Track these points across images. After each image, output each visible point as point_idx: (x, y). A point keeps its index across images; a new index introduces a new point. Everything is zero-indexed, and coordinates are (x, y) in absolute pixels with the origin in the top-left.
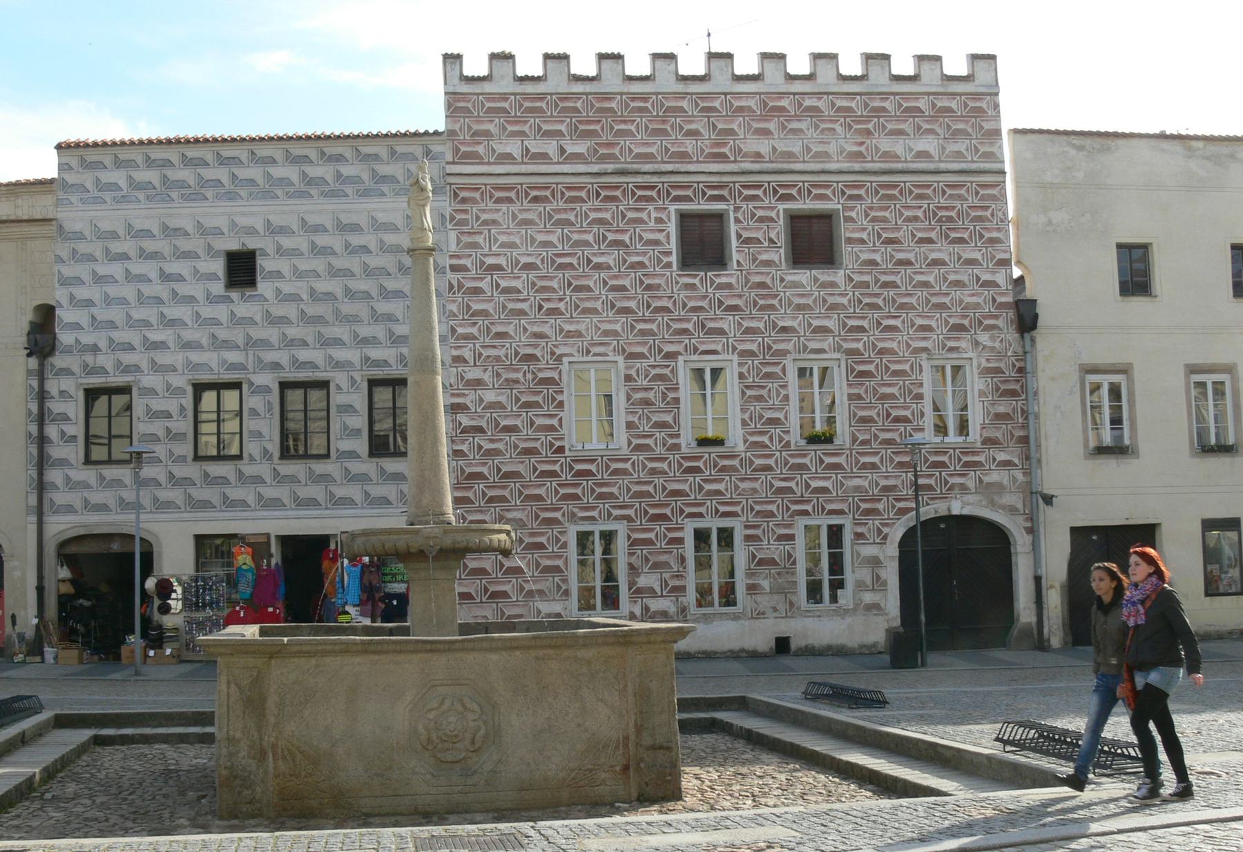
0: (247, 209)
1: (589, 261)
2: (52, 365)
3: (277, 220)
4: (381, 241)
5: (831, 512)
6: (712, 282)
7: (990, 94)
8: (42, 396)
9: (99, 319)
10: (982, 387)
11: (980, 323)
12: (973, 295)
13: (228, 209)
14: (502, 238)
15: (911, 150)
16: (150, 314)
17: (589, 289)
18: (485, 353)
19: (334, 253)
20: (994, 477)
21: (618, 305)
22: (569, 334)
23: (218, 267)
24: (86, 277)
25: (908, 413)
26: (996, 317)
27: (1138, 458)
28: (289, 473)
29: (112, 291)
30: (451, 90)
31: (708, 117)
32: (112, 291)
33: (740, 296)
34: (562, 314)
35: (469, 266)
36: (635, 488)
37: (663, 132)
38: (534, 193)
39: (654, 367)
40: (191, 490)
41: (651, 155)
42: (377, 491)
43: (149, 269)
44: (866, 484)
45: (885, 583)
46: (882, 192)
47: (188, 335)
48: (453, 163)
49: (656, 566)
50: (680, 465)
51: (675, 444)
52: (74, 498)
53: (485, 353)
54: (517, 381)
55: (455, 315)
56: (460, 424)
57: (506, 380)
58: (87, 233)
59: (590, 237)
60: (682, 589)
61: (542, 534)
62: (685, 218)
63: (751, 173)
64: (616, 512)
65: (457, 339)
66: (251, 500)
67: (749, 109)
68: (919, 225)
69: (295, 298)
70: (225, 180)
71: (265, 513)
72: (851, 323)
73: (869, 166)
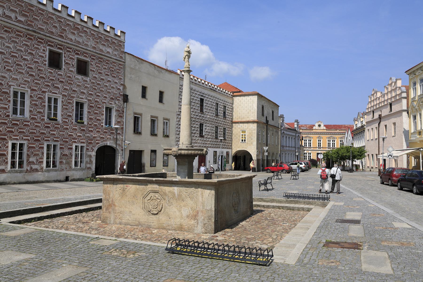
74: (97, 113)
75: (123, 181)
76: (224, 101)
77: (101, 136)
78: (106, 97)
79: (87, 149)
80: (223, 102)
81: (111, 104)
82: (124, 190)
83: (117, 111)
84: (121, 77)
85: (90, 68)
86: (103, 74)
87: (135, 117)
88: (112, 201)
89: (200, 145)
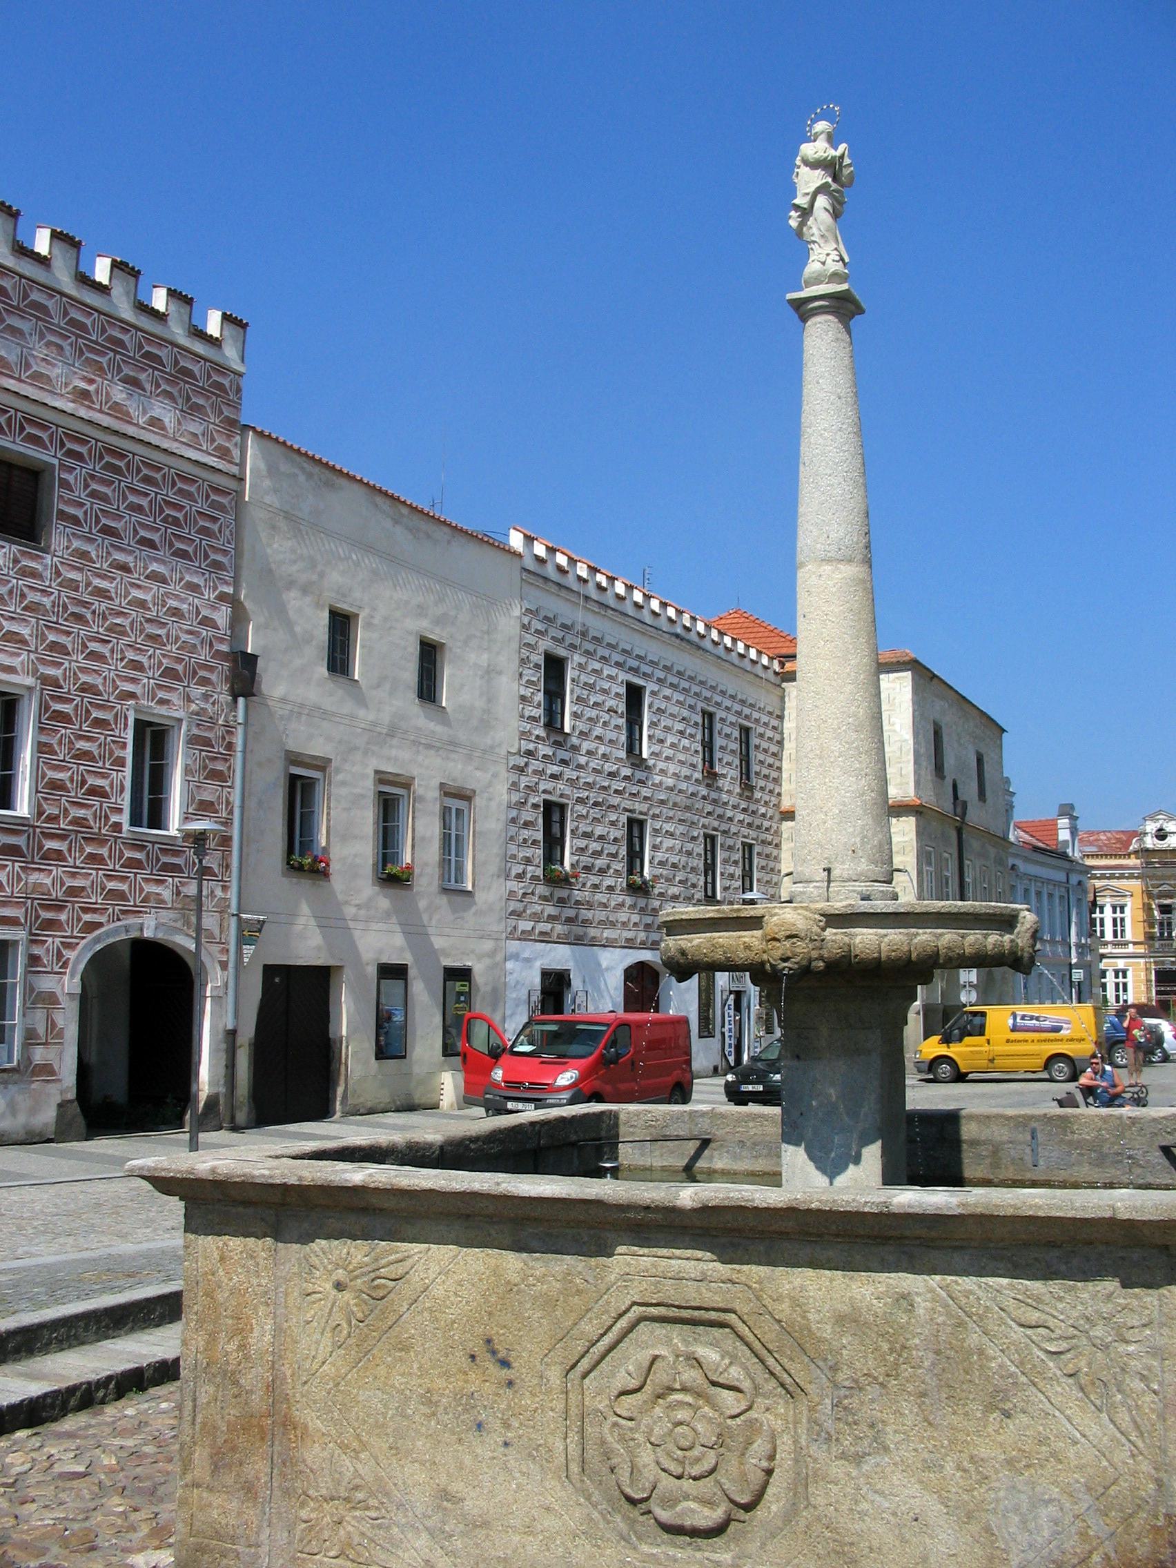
27: (284, 875)
44: (48, 881)
45: (60, 1034)
74: (85, 755)
75: (365, 1210)
76: (743, 702)
77: (111, 885)
78: (137, 666)
79: (34, 960)
80: (737, 707)
81: (162, 702)
82: (376, 1296)
83: (193, 740)
84: (219, 558)
85: (58, 505)
86: (128, 540)
87: (293, 779)
88: (271, 1388)
89: (630, 935)
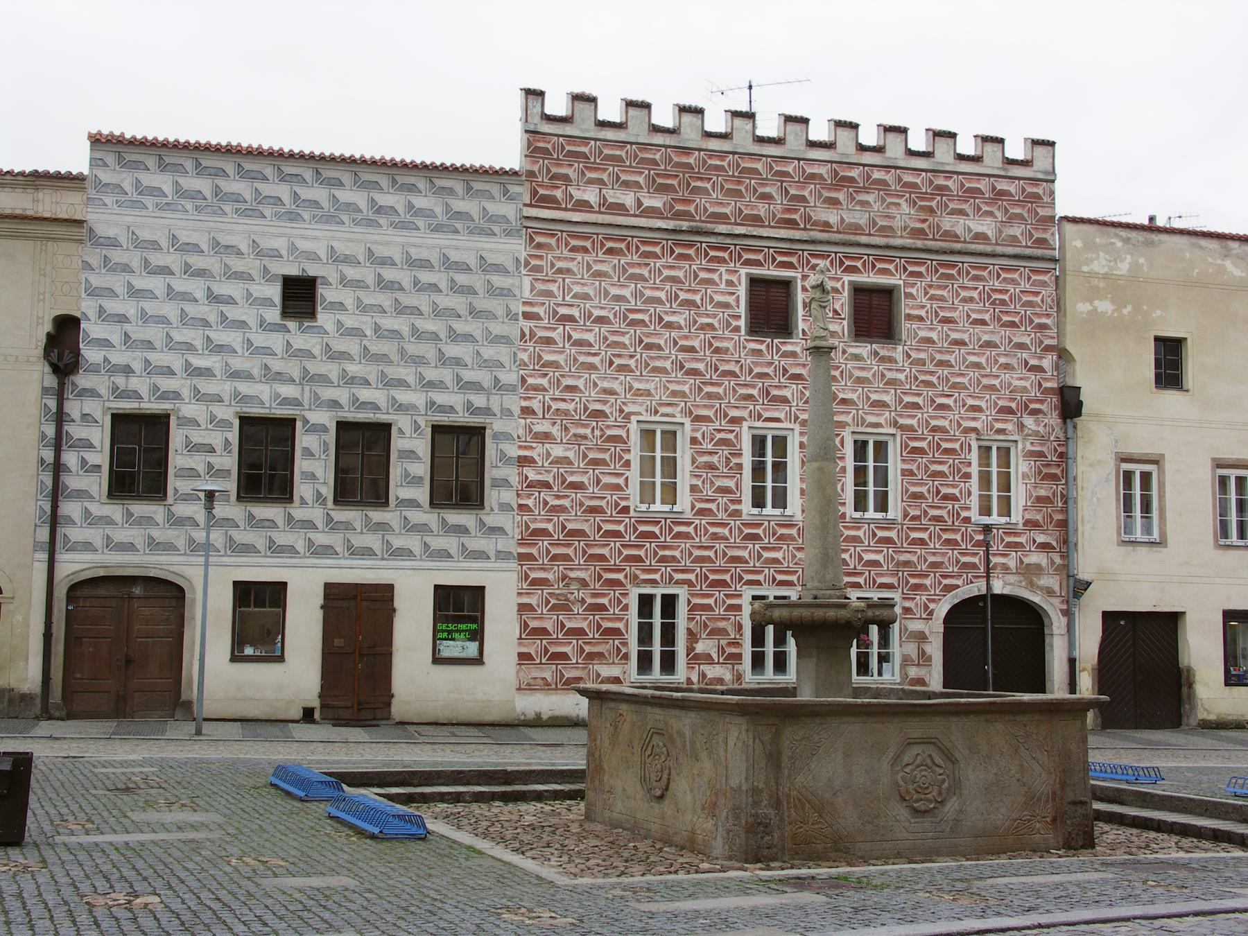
0: (309, 232)
1: (661, 319)
2: (73, 384)
3: (341, 247)
4: (452, 280)
5: (882, 586)
6: (778, 350)
7: (1047, 181)
8: (60, 418)
9: (134, 337)
10: (1026, 469)
11: (1027, 406)
12: (1021, 379)
13: (288, 231)
14: (576, 289)
15: (970, 230)
16: (194, 336)
17: (659, 348)
18: (555, 406)
19: (402, 289)
20: (1035, 558)
21: (688, 365)
22: (639, 393)
23: (274, 292)
24: (120, 289)
25: (956, 491)
26: (1041, 402)
28: (344, 520)
29: (151, 307)
30: (532, 128)
31: (782, 182)
32: (151, 307)
33: (804, 366)
34: (632, 371)
35: (542, 314)
36: (697, 553)
37: (738, 193)
38: (609, 245)
39: (719, 431)
40: (233, 533)
41: (725, 216)
42: (437, 543)
43: (196, 287)
45: (929, 659)
46: (941, 271)
47: (237, 363)
48: (530, 205)
49: (714, 632)
50: (741, 531)
51: (737, 511)
52: (94, 535)
53: (555, 406)
54: (585, 437)
55: (525, 365)
56: (527, 477)
57: (575, 435)
58: (123, 240)
59: (662, 295)
60: (739, 657)
61: (604, 595)
62: (755, 283)
63: (821, 242)
64: (677, 576)
65: (527, 389)
66: (300, 546)
67: (821, 177)
68: (973, 306)
69: (356, 332)
70: (286, 198)
71: (316, 561)
72: (907, 399)
73: (930, 244)
